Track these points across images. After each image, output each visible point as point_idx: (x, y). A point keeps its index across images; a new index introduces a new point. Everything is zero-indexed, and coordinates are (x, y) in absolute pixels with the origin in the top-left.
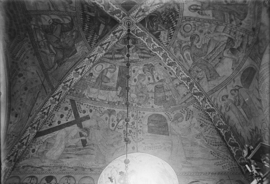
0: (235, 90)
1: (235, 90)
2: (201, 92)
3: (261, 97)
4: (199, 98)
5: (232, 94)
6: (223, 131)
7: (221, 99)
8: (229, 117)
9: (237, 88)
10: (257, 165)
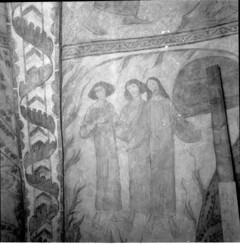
0: (143, 88)
1: (143, 88)
2: (50, 39)
3: (196, 111)
4: (26, 56)
5: (127, 94)
6: (38, 197)
7: (88, 91)
8: (76, 159)
9: (152, 86)
10: (50, 143)
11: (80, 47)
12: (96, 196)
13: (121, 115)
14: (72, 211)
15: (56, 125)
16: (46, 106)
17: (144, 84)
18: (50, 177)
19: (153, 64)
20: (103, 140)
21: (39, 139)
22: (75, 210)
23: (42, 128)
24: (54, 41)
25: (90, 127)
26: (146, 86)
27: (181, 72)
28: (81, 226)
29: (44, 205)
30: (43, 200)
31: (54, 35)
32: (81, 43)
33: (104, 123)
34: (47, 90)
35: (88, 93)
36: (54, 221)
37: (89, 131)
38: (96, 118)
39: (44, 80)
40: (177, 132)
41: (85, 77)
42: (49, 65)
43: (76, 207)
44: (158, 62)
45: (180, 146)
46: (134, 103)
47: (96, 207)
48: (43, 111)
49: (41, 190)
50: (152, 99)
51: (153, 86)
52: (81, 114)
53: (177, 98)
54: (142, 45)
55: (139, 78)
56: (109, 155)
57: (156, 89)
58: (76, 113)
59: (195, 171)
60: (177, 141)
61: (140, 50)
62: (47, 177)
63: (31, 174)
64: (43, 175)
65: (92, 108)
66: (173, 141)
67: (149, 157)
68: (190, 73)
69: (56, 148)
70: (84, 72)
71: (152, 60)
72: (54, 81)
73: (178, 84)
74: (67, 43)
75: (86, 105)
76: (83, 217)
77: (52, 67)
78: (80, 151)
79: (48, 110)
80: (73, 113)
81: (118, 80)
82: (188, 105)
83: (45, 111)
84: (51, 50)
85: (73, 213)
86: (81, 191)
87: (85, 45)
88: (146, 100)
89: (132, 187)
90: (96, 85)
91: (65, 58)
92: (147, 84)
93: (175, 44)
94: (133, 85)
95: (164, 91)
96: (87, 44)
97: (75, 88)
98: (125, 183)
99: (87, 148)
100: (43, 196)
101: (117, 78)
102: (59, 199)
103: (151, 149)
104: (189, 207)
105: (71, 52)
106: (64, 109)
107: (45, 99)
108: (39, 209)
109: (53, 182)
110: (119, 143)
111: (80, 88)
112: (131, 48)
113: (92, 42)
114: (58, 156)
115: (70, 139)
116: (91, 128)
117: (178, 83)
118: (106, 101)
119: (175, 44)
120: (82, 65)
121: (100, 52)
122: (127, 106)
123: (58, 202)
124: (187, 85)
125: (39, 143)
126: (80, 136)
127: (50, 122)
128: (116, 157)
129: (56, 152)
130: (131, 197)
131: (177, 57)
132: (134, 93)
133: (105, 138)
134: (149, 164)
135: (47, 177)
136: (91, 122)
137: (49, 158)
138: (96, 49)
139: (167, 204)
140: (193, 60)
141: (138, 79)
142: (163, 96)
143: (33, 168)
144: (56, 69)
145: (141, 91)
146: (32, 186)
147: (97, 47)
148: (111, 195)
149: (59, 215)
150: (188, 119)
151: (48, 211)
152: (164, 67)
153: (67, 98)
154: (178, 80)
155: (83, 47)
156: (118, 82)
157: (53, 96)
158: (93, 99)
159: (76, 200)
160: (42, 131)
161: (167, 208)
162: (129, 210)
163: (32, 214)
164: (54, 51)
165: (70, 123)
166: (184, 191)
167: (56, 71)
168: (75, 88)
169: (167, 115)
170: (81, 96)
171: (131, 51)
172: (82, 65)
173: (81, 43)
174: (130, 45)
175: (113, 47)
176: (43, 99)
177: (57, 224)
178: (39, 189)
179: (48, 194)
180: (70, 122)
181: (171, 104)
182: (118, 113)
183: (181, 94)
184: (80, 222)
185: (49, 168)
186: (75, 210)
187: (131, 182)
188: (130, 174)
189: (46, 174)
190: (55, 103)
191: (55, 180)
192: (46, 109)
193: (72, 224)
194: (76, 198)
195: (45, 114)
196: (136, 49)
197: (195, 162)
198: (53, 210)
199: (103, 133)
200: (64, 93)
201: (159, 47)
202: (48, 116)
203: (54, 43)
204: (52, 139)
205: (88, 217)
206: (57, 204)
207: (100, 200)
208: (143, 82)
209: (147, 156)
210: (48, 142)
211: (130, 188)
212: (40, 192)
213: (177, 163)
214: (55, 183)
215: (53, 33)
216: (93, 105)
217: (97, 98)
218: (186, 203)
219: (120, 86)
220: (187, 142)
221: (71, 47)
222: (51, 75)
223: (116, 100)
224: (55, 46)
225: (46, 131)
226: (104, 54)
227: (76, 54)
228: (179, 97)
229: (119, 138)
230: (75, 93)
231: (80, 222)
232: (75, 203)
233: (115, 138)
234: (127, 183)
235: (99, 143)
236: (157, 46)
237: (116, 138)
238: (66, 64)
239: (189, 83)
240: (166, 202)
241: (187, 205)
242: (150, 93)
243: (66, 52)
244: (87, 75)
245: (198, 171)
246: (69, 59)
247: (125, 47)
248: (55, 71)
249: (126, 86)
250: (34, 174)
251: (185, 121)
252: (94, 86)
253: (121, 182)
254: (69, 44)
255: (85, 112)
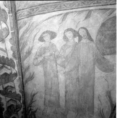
0: (76, 34)
2: (4, 10)
5: (65, 38)
6: (8, 101)
7: (38, 37)
8: (32, 77)
9: (82, 33)
10: (13, 74)
11: (31, 10)
12: (45, 98)
13: (60, 51)
14: (30, 106)
15: (16, 64)
16: (7, 53)
17: (76, 31)
18: (14, 91)
19: (84, 18)
20: (49, 66)
21: (5, 72)
22: (32, 105)
23: (6, 66)
24: (7, 12)
25: (40, 59)
26: (78, 33)
27: (103, 25)
28: (36, 113)
29: (12, 105)
30: (11, 103)
31: (7, 7)
32: (31, 7)
33: (49, 56)
34: (6, 44)
35: (38, 38)
36: (20, 113)
37: (39, 61)
38: (44, 53)
39: (4, 38)
40: (97, 64)
41: (36, 29)
42: (5, 28)
43: (33, 104)
44: (88, 17)
45: (99, 73)
46: (69, 44)
47: (45, 104)
48: (6, 56)
49: (10, 98)
50: (82, 41)
51: (83, 33)
52: (34, 51)
53: (98, 42)
54: (77, 5)
55: (73, 27)
56: (52, 75)
57: (85, 35)
58: (30, 51)
59: (108, 91)
60: (97, 70)
61: (75, 9)
62: (13, 91)
63: (3, 90)
64: (11, 90)
65: (41, 47)
66: (94, 67)
67: (78, 78)
68: (109, 25)
69: (17, 76)
70: (34, 25)
71: (83, 15)
72: (11, 38)
73: (100, 33)
74: (20, 8)
75: (37, 46)
76: (37, 109)
77: (8, 29)
78: (34, 73)
79: (8, 56)
80: (28, 52)
81: (59, 29)
82: (106, 48)
83: (7, 56)
84: (6, 18)
85: (31, 106)
86: (35, 96)
87: (34, 7)
88: (78, 42)
89: (67, 96)
90: (44, 33)
91: (20, 18)
92: (78, 32)
93: (101, 4)
94: (69, 32)
95: (90, 37)
96: (36, 7)
97: (29, 36)
98: (62, 93)
99: (39, 71)
100: (11, 101)
101: (58, 27)
102: (21, 101)
103: (79, 73)
104: (102, 113)
105: (24, 14)
106: (20, 40)
107: (6, 49)
108: (10, 107)
109: (17, 94)
110: (59, 68)
111: (33, 36)
112: (69, 7)
113: (39, 5)
114: (19, 80)
115: (27, 67)
116: (41, 59)
117: (100, 32)
118: (50, 42)
119: (101, 4)
120: (33, 21)
121: (46, 11)
122: (65, 45)
123: (21, 103)
124: (106, 34)
125: (6, 74)
126: (34, 64)
127: (12, 62)
128: (57, 77)
129: (18, 78)
130: (66, 101)
131: (101, 13)
132: (70, 37)
133: (50, 65)
134: (78, 82)
135: (13, 91)
136: (40, 55)
137: (13, 81)
138: (43, 9)
139: (88, 108)
140: (112, 17)
141: (73, 28)
142: (89, 39)
143: (3, 87)
144: (11, 31)
145: (75, 36)
146: (4, 96)
147: (44, 8)
148: (53, 99)
149: (22, 110)
150: (105, 57)
151: (15, 108)
152: (91, 20)
153: (23, 43)
154: (100, 30)
155: (33, 10)
156: (59, 30)
157: (12, 48)
158: (42, 42)
159: (32, 100)
160: (6, 68)
161: (88, 111)
162: (64, 108)
163: (5, 109)
164: (8, 19)
165: (26, 58)
166: (100, 102)
167: (12, 32)
168: (29, 36)
169: (91, 52)
170: (34, 41)
171: (68, 10)
172: (33, 21)
173: (31, 7)
174: (68, 6)
175: (56, 7)
176: (5, 50)
177: (21, 114)
178: (8, 97)
179: (15, 100)
180: (26, 57)
181: (94, 46)
182: (59, 49)
183: (102, 39)
184: (35, 112)
185: (14, 87)
186: (32, 105)
187: (66, 92)
188: (66, 87)
189: (12, 90)
190: (13, 51)
191: (18, 92)
192: (7, 55)
193: (30, 112)
194: (33, 99)
195: (7, 58)
196: (72, 8)
197: (108, 86)
198: (18, 107)
199: (49, 62)
200: (21, 41)
201: (89, 7)
202: (9, 59)
203: (7, 13)
204: (14, 71)
205: (40, 109)
206: (20, 104)
207: (47, 101)
208: (76, 30)
209: (77, 77)
210: (11, 73)
211: (66, 96)
212: (9, 99)
213: (96, 84)
214: (18, 94)
215: (5, 6)
216: (42, 45)
217: (45, 41)
218: (100, 110)
219: (61, 32)
220: (104, 72)
221: (23, 10)
222: (8, 34)
223: (58, 42)
224: (8, 15)
225: (9, 67)
226: (49, 12)
227: (28, 15)
228: (100, 41)
229: (59, 65)
230: (29, 40)
231: (35, 112)
232: (32, 102)
233: (56, 65)
234: (64, 93)
235: (46, 68)
236: (88, 6)
237: (57, 65)
238: (20, 22)
239: (108, 32)
240: (87, 107)
241: (101, 111)
242: (80, 38)
243: (20, 15)
244: (37, 28)
245: (110, 92)
246: (23, 19)
247: (64, 7)
248: (10, 32)
249: (64, 33)
250: (4, 90)
251: (104, 58)
252: (42, 34)
253: (60, 92)
254: (22, 9)
255: (37, 50)
